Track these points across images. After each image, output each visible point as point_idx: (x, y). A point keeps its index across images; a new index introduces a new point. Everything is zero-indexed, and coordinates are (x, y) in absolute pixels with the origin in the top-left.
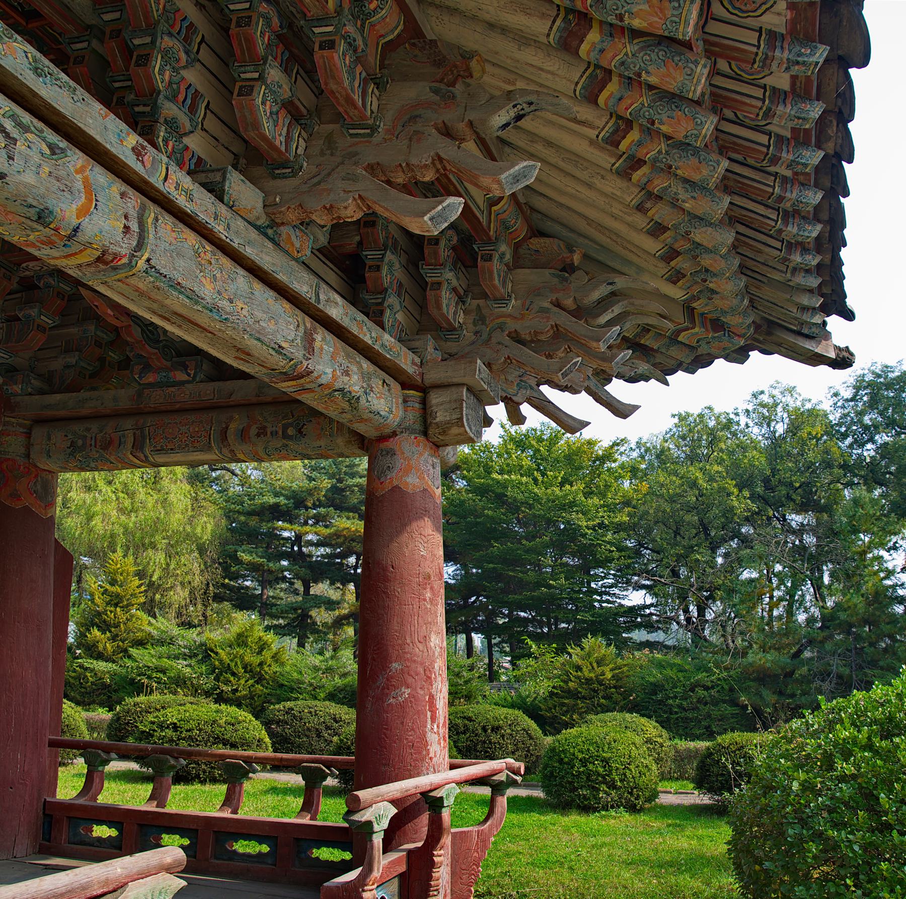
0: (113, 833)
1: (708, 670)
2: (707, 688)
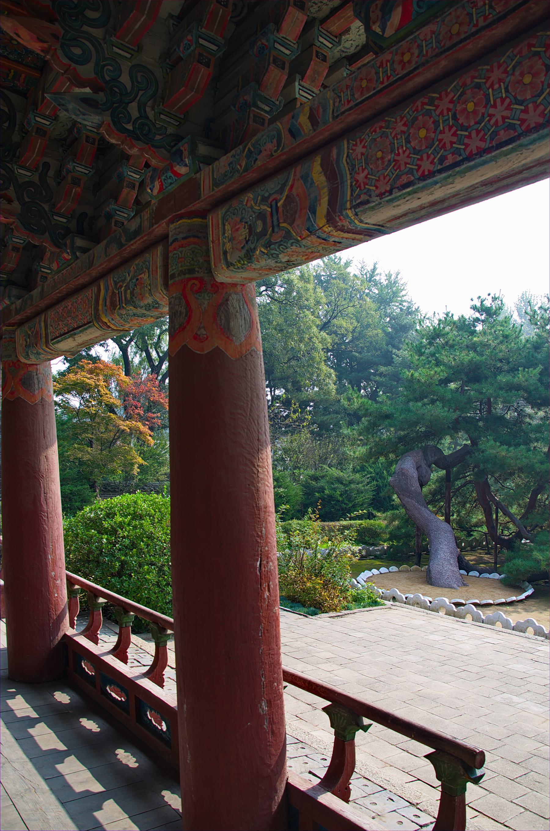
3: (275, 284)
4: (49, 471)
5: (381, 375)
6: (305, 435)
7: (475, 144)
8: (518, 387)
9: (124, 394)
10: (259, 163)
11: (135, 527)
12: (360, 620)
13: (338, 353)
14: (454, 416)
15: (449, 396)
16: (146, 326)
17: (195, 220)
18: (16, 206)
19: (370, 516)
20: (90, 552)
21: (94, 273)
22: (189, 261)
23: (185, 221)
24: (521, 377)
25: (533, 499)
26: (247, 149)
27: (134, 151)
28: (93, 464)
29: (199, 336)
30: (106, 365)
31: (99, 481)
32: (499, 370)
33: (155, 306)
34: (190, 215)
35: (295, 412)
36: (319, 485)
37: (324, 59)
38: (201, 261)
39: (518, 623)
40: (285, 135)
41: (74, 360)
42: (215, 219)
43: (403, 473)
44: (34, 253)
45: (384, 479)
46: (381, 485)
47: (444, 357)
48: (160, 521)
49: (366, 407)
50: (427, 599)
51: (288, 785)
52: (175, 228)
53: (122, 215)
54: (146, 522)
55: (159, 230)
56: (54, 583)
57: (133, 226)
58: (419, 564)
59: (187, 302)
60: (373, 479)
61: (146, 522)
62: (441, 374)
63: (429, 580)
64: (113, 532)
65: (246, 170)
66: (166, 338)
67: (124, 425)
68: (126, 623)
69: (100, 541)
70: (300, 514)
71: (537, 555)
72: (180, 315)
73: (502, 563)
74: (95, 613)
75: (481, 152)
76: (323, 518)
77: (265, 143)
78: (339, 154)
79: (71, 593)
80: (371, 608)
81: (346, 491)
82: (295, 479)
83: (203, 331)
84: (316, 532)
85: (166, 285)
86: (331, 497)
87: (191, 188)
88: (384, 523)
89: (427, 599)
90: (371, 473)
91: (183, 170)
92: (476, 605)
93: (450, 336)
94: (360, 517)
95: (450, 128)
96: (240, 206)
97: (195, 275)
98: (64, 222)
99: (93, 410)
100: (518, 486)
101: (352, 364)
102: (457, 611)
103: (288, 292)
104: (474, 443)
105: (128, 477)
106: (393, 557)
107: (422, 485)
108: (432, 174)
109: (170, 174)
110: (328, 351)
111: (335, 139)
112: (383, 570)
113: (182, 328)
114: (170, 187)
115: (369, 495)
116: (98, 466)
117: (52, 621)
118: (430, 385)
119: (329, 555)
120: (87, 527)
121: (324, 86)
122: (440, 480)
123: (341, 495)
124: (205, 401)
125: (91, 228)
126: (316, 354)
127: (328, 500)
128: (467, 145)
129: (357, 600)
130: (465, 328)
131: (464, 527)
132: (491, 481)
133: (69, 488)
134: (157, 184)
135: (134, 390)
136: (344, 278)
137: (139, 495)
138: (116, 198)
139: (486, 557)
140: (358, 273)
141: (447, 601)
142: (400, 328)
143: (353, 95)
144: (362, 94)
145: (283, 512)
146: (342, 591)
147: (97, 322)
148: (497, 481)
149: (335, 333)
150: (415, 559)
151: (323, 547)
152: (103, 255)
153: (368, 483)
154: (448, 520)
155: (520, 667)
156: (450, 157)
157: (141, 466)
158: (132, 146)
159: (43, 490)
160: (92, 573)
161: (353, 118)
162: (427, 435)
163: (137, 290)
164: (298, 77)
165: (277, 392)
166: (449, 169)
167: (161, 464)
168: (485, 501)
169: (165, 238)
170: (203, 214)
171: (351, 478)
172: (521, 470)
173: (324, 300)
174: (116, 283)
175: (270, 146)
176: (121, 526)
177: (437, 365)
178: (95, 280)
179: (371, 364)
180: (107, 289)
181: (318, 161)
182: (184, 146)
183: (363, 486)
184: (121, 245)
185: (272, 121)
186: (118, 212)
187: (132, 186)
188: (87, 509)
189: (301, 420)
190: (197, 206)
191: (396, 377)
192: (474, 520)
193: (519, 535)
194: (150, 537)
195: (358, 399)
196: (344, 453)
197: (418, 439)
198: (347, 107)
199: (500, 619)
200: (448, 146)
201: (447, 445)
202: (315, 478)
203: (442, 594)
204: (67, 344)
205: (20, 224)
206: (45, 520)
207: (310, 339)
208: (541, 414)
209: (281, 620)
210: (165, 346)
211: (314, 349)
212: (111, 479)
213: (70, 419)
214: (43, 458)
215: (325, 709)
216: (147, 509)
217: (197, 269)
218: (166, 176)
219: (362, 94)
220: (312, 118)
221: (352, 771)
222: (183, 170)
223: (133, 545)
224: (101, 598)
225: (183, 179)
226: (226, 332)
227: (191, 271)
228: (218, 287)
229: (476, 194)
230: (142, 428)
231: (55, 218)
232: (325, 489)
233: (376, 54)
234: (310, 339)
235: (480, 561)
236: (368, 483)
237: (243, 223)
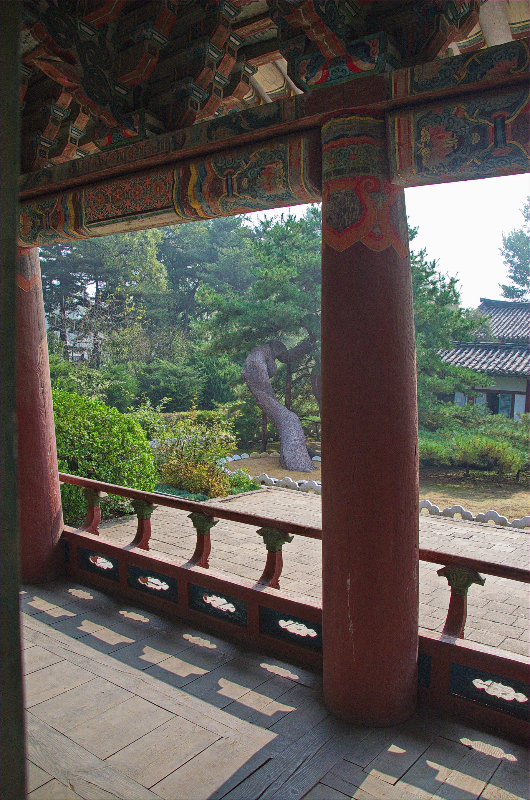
6: (138, 328)
17: (367, 118)
18: (79, 68)
22: (363, 159)
23: (357, 118)
26: (469, 61)
29: (375, 234)
36: (153, 377)
38: (375, 160)
45: (214, 371)
46: (212, 378)
49: (219, 302)
56: (53, 480)
60: (204, 371)
62: (293, 274)
63: (283, 464)
68: (147, 515)
72: (353, 211)
74: (95, 508)
77: (499, 59)
80: (251, 492)
81: (180, 383)
83: (378, 230)
87: (377, 86)
90: (202, 366)
91: (365, 66)
96: (446, 115)
98: (123, 94)
114: (337, 81)
117: (53, 519)
123: (176, 387)
130: (307, 231)
134: (319, 75)
145: (165, 404)
150: (261, 447)
153: (201, 375)
159: (40, 383)
171: (184, 370)
186: (194, 92)
203: (300, 478)
205: (83, 90)
206: (43, 415)
214: (39, 350)
215: (440, 573)
217: (371, 168)
218: (338, 69)
224: (102, 492)
225: (360, 75)
231: (117, 88)
232: (160, 382)
236: (201, 375)
237: (451, 132)
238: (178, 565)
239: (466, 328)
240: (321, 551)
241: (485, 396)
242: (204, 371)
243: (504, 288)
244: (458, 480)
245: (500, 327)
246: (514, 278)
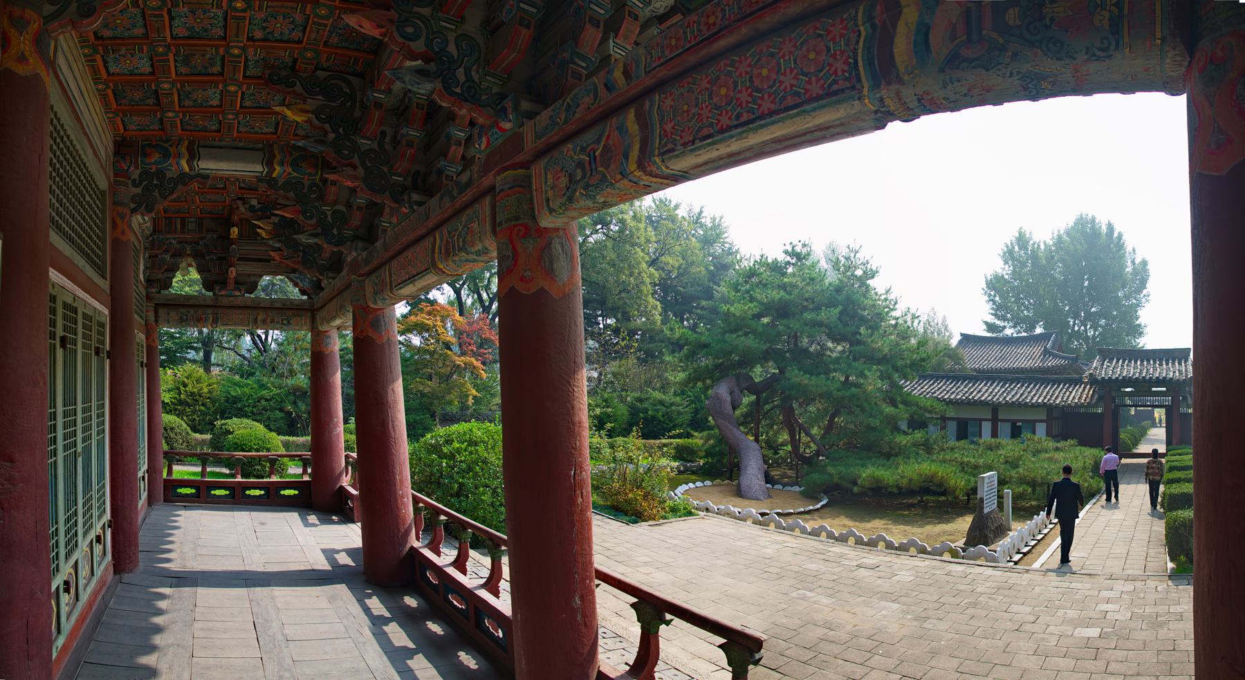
0: (193, 491)
1: (268, 388)
2: (266, 400)
3: (611, 222)
4: (395, 402)
5: (702, 308)
6: (632, 361)
7: (767, 105)
8: (821, 324)
9: (459, 333)
10: (577, 115)
11: (471, 453)
12: (677, 528)
13: (665, 288)
14: (765, 347)
15: (760, 329)
16: (477, 270)
19: (689, 436)
20: (432, 474)
21: (430, 225)
24: (823, 315)
25: (831, 421)
27: (463, 112)
28: (433, 395)
30: (442, 307)
31: (439, 411)
32: (805, 308)
33: (485, 251)
34: (514, 167)
35: (623, 339)
37: (636, 18)
39: (814, 529)
40: (601, 89)
41: (415, 303)
42: (537, 169)
43: (717, 398)
44: (374, 210)
47: (759, 294)
48: (493, 448)
50: (736, 510)
51: (599, 672)
52: (501, 180)
53: (452, 170)
54: (481, 448)
55: (486, 182)
57: (464, 178)
58: (730, 479)
59: (514, 248)
60: (692, 402)
61: (481, 448)
63: (739, 493)
64: (451, 456)
65: (565, 122)
66: (495, 280)
67: (460, 361)
69: (440, 465)
70: (626, 432)
71: (830, 469)
73: (802, 477)
75: (772, 113)
76: (645, 436)
78: (651, 106)
79: (417, 510)
82: (622, 400)
84: (639, 449)
85: (494, 232)
86: (654, 418)
87: (516, 141)
88: (700, 442)
89: (736, 510)
91: (507, 126)
92: (778, 514)
93: (764, 276)
94: (679, 436)
95: (747, 89)
97: (521, 222)
99: (432, 348)
100: (818, 410)
101: (677, 297)
102: (763, 520)
103: (621, 231)
104: (782, 372)
105: (464, 407)
106: (707, 473)
107: (734, 408)
108: (729, 128)
109: (495, 130)
110: (655, 285)
111: (648, 92)
112: (699, 484)
113: (510, 271)
115: (688, 417)
116: (437, 398)
118: (744, 319)
119: (649, 469)
120: (429, 452)
121: (637, 44)
122: (751, 404)
124: (531, 341)
125: (425, 184)
126: (644, 288)
127: (650, 421)
128: (760, 106)
129: (674, 510)
131: (772, 446)
132: (795, 405)
133: (412, 417)
134: (484, 140)
135: (467, 328)
136: (673, 219)
137: (474, 424)
138: (446, 156)
139: (789, 472)
140: (686, 215)
141: (754, 511)
142: (721, 266)
143: (663, 52)
144: (671, 52)
146: (660, 502)
147: (433, 269)
148: (800, 406)
149: (663, 269)
150: (728, 474)
151: (644, 463)
152: (437, 207)
154: (757, 440)
155: (813, 567)
156: (745, 115)
157: (475, 397)
158: (461, 108)
160: (434, 493)
161: (663, 73)
162: (741, 364)
163: (469, 238)
164: (612, 35)
165: (609, 321)
166: (745, 124)
167: (493, 396)
168: (791, 425)
169: (492, 189)
170: (526, 165)
172: (821, 396)
173: (654, 239)
174: (449, 233)
175: (588, 100)
176: (458, 451)
177: (751, 301)
178: (431, 232)
179: (694, 298)
180: (441, 239)
181: (631, 115)
182: (508, 104)
183: (682, 408)
184: (453, 198)
185: (588, 76)
187: (459, 143)
188: (429, 436)
189: (628, 347)
190: (520, 158)
191: (714, 311)
192: (780, 440)
193: (818, 453)
194: (485, 462)
195: (679, 330)
196: (666, 379)
197: (731, 366)
198: (657, 63)
199: (798, 526)
200: (744, 104)
201: (758, 373)
202: (640, 400)
204: (409, 290)
207: (639, 273)
208: (840, 348)
209: (595, 530)
210: (494, 288)
211: (643, 282)
212: (448, 409)
213: (412, 356)
215: (633, 605)
216: (483, 435)
219: (671, 52)
220: (626, 73)
221: (657, 659)
222: (507, 126)
223: (470, 469)
225: (508, 134)
226: (550, 273)
227: (517, 218)
228: (542, 232)
229: (767, 149)
230: (475, 362)
233: (683, 14)
234: (639, 273)
235: (784, 476)
238: (469, 586)
239: (923, 360)
240: (242, 569)
241: (955, 423)
242: (692, 402)
243: (986, 323)
244: (910, 506)
245: (975, 360)
246: (995, 315)
